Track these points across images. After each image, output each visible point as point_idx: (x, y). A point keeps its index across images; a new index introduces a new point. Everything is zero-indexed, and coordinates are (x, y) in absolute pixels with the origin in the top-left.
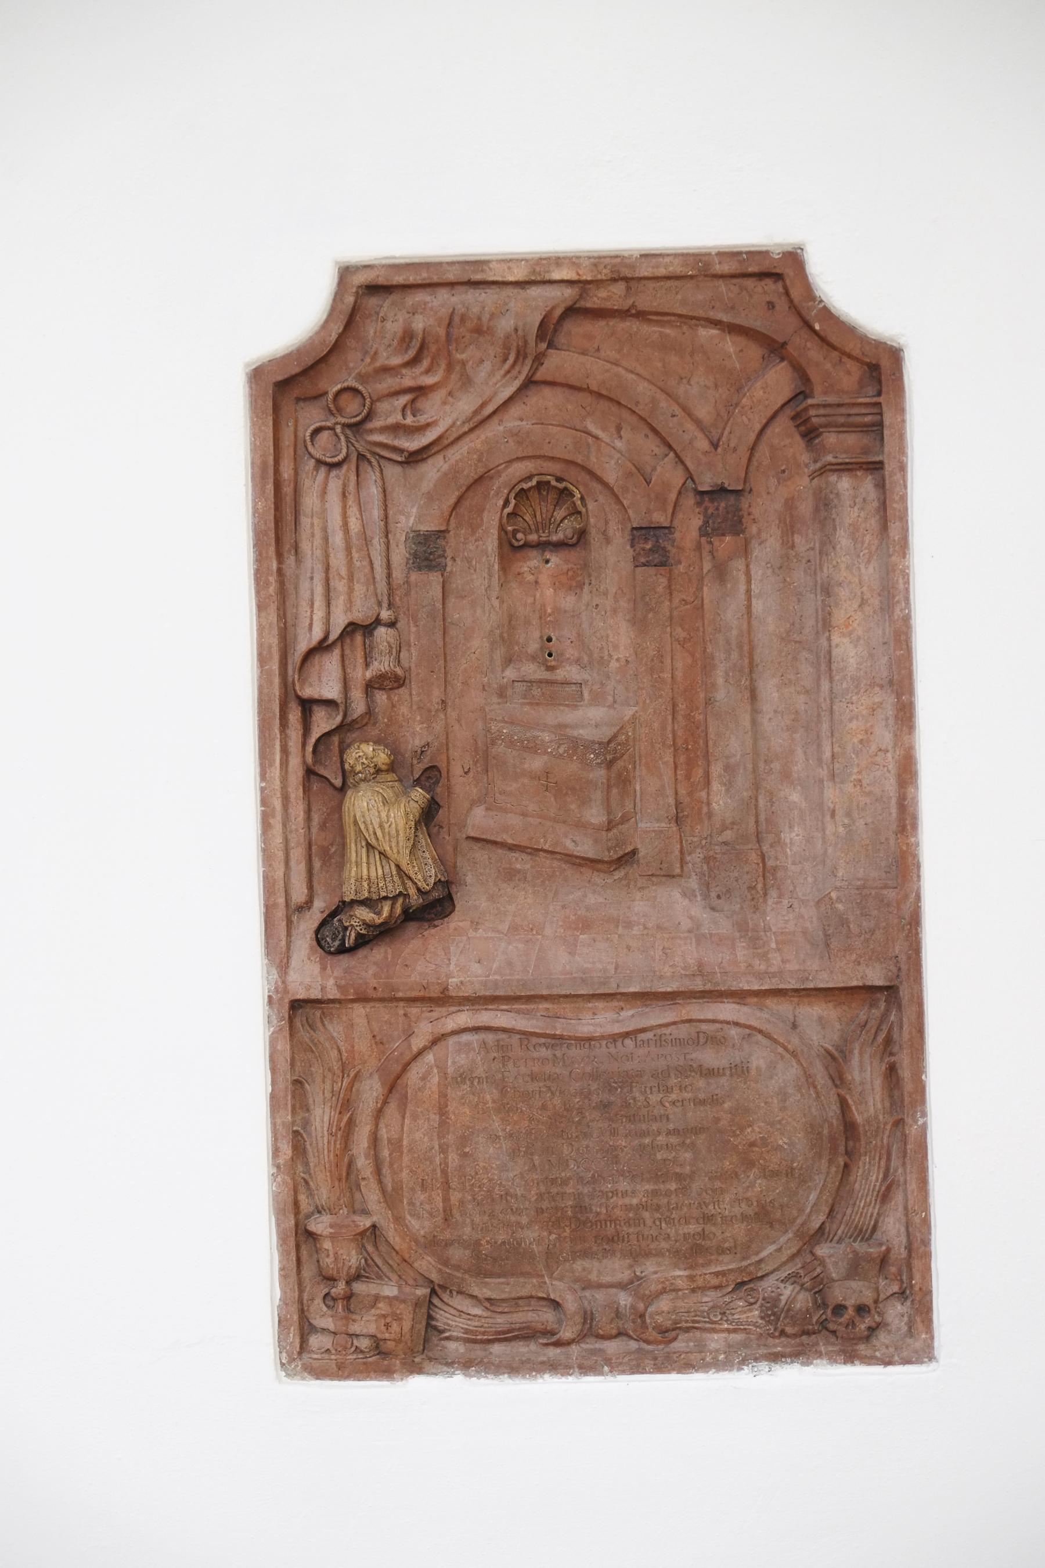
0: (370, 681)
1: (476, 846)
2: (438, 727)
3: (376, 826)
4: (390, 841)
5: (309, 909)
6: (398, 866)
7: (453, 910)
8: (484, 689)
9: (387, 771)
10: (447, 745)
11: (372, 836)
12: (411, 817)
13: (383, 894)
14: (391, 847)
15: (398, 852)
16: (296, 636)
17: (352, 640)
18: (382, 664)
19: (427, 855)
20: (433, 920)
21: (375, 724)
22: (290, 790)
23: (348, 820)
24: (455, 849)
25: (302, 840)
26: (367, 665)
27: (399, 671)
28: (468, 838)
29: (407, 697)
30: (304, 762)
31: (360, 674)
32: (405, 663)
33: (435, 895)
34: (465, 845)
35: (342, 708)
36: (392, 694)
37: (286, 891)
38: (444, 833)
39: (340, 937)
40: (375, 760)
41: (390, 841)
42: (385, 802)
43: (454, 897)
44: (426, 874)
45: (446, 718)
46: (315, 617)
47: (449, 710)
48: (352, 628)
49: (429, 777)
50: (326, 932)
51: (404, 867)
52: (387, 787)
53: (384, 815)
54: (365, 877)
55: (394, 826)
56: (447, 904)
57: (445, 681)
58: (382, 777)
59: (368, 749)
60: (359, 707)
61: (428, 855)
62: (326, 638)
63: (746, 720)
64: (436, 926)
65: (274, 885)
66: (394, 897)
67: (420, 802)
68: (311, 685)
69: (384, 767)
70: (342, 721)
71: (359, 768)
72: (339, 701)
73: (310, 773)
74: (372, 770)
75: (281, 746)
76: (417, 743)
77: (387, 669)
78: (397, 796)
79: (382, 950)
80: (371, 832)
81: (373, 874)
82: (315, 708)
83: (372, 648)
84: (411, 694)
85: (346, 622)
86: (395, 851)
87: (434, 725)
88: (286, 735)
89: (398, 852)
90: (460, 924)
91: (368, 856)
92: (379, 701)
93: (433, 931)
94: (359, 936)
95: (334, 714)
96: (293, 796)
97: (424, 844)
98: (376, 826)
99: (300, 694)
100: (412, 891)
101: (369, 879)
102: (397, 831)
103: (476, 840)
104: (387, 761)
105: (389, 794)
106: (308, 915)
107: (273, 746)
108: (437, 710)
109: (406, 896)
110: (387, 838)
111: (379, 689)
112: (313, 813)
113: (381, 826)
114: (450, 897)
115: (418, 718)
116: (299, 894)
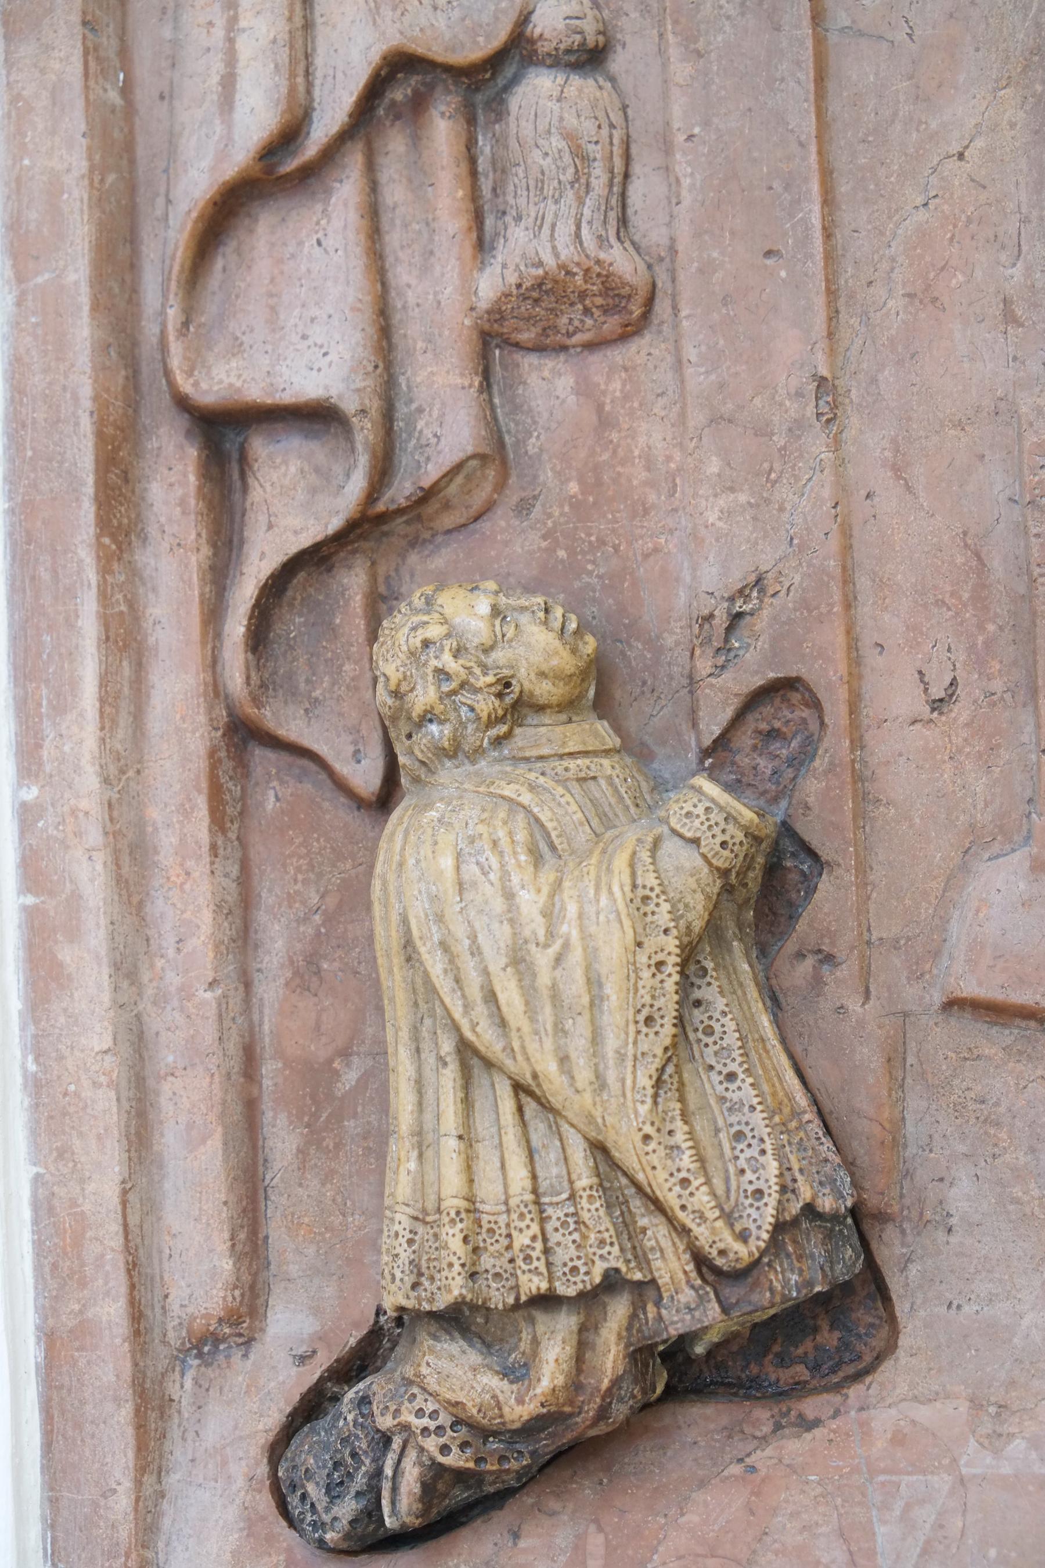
0: (497, 313)
1: (993, 1042)
2: (806, 502)
3: (496, 963)
4: (559, 1029)
5: (249, 1342)
6: (599, 1149)
7: (891, 1347)
8: (1009, 317)
9: (569, 707)
10: (847, 579)
11: (481, 1011)
12: (663, 916)
13: (534, 1284)
14: (564, 1060)
15: (600, 1083)
16: (172, 138)
17: (416, 140)
18: (546, 236)
19: (745, 1091)
20: (798, 1390)
21: (524, 508)
22: (154, 813)
23: (386, 937)
24: (895, 1058)
25: (209, 1034)
26: (482, 246)
27: (622, 262)
28: (954, 1004)
29: (666, 377)
30: (216, 689)
31: (446, 292)
32: (649, 228)
33: (787, 1282)
34: (940, 1040)
35: (365, 433)
36: (597, 363)
37: (133, 1268)
38: (841, 985)
39: (360, 1481)
40: (499, 656)
41: (559, 1029)
42: (542, 848)
43: (895, 1284)
44: (731, 1180)
45: (841, 463)
46: (245, 48)
47: (853, 423)
48: (401, 81)
49: (773, 734)
50: (309, 1453)
51: (628, 1151)
52: (558, 776)
53: (530, 902)
54: (453, 1203)
55: (576, 956)
56: (863, 1316)
57: (832, 293)
58: (539, 735)
59: (469, 611)
60: (445, 427)
61: (746, 1087)
62: (289, 136)
63: (582, 1126)
64: (808, 1425)
65: (78, 1242)
66: (583, 1296)
67: (710, 844)
68: (237, 348)
69: (545, 690)
70: (372, 495)
71: (424, 696)
72: (349, 405)
73: (243, 736)
74: (486, 705)
75: (106, 621)
76: (707, 578)
77: (567, 252)
78: (606, 821)
79: (563, 1537)
80: (475, 992)
81: (489, 1190)
82: (261, 447)
83: (502, 169)
84: (679, 365)
85: (375, 56)
86: (584, 1076)
87: (784, 493)
88: (134, 573)
89: (600, 1083)
90: (923, 1413)
91: (467, 1102)
92: (540, 404)
93: (795, 1447)
94: (437, 1476)
95: (338, 469)
96: (167, 842)
97: (732, 1039)
98: (496, 963)
99: (186, 386)
100: (671, 1267)
101: (472, 1206)
102: (594, 982)
103: (994, 1012)
104: (565, 661)
105: (562, 810)
106: (238, 1370)
107: (71, 622)
108: (796, 429)
109: (645, 1290)
110: (547, 1015)
111: (539, 349)
112: (261, 916)
113: (519, 961)
114: (873, 1283)
115: (714, 466)
116: (198, 1278)
